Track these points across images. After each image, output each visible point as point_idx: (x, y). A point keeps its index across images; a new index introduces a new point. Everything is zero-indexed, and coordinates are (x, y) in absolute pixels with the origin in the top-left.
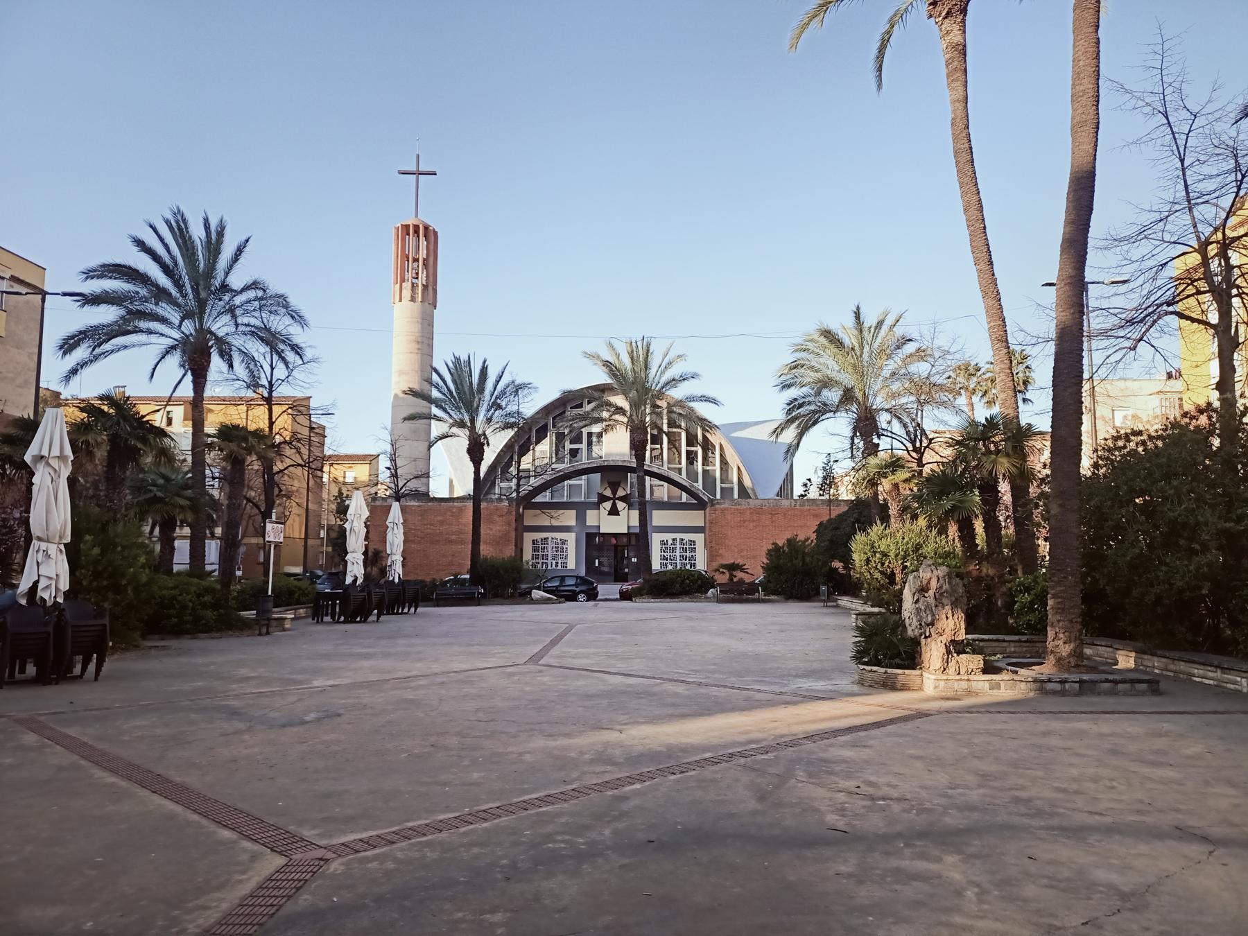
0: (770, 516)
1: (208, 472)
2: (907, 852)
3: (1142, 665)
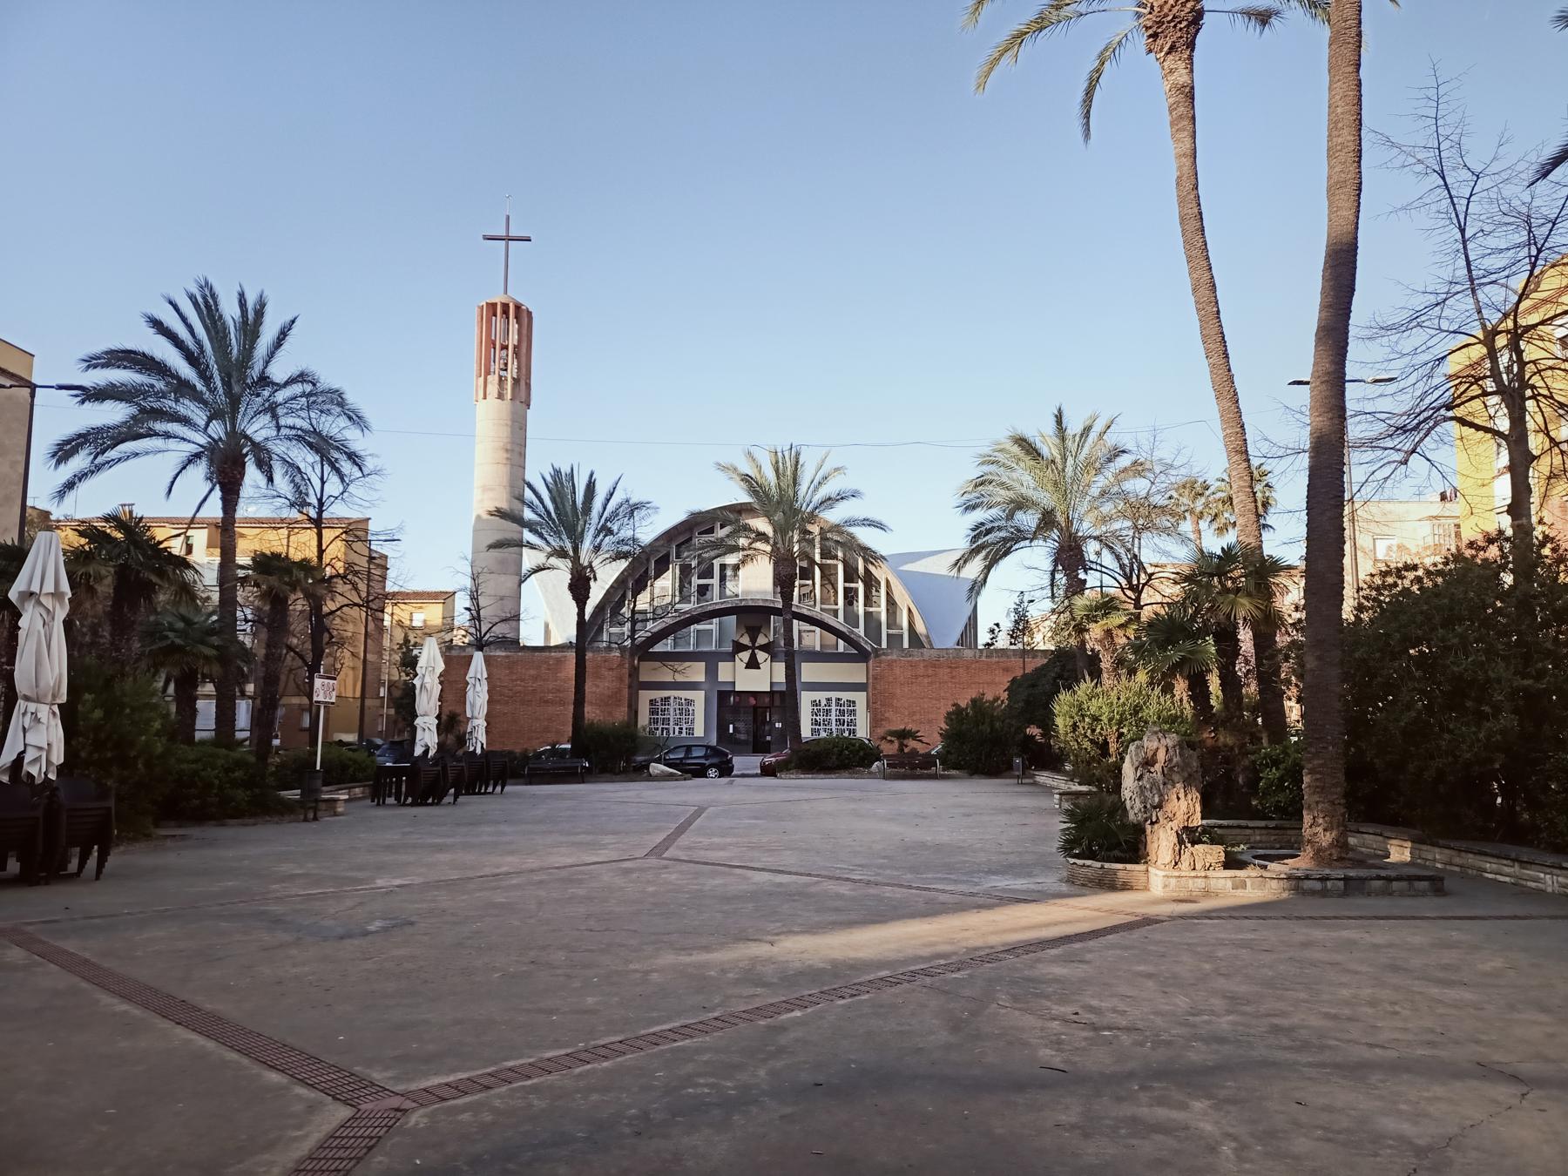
0: (948, 670)
1: (239, 614)
2: (1144, 1097)
3: (1420, 858)
